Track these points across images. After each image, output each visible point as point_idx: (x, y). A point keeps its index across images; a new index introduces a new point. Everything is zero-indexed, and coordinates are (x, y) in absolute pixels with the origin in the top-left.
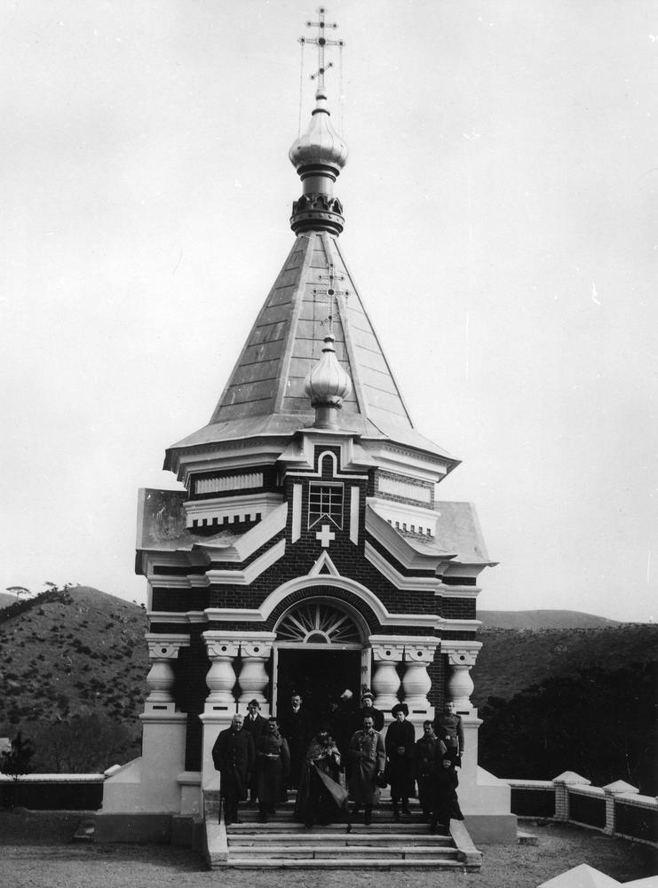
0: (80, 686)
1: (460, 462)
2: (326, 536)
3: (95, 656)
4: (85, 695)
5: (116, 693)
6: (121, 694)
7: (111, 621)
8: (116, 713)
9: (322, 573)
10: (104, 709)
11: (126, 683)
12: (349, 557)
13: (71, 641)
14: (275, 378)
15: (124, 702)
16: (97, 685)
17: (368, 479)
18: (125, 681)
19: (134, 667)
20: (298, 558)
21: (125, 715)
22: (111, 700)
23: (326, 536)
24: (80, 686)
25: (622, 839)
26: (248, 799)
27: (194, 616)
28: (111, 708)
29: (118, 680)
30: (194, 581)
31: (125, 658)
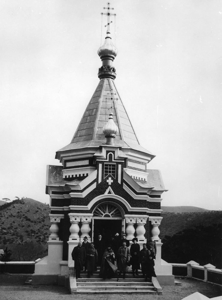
0: (27, 232)
1: (155, 156)
2: (110, 181)
3: (32, 222)
4: (29, 235)
5: (39, 234)
6: (41, 234)
7: (37, 210)
9: (109, 194)
12: (118, 188)
13: (24, 216)
15: (42, 237)
16: (33, 231)
17: (124, 162)
18: (42, 230)
19: (45, 225)
20: (101, 189)
21: (42, 242)
22: (37, 237)
23: (110, 181)
24: (27, 232)
27: (65, 208)
28: (38, 239)
30: (66, 196)
31: (42, 222)
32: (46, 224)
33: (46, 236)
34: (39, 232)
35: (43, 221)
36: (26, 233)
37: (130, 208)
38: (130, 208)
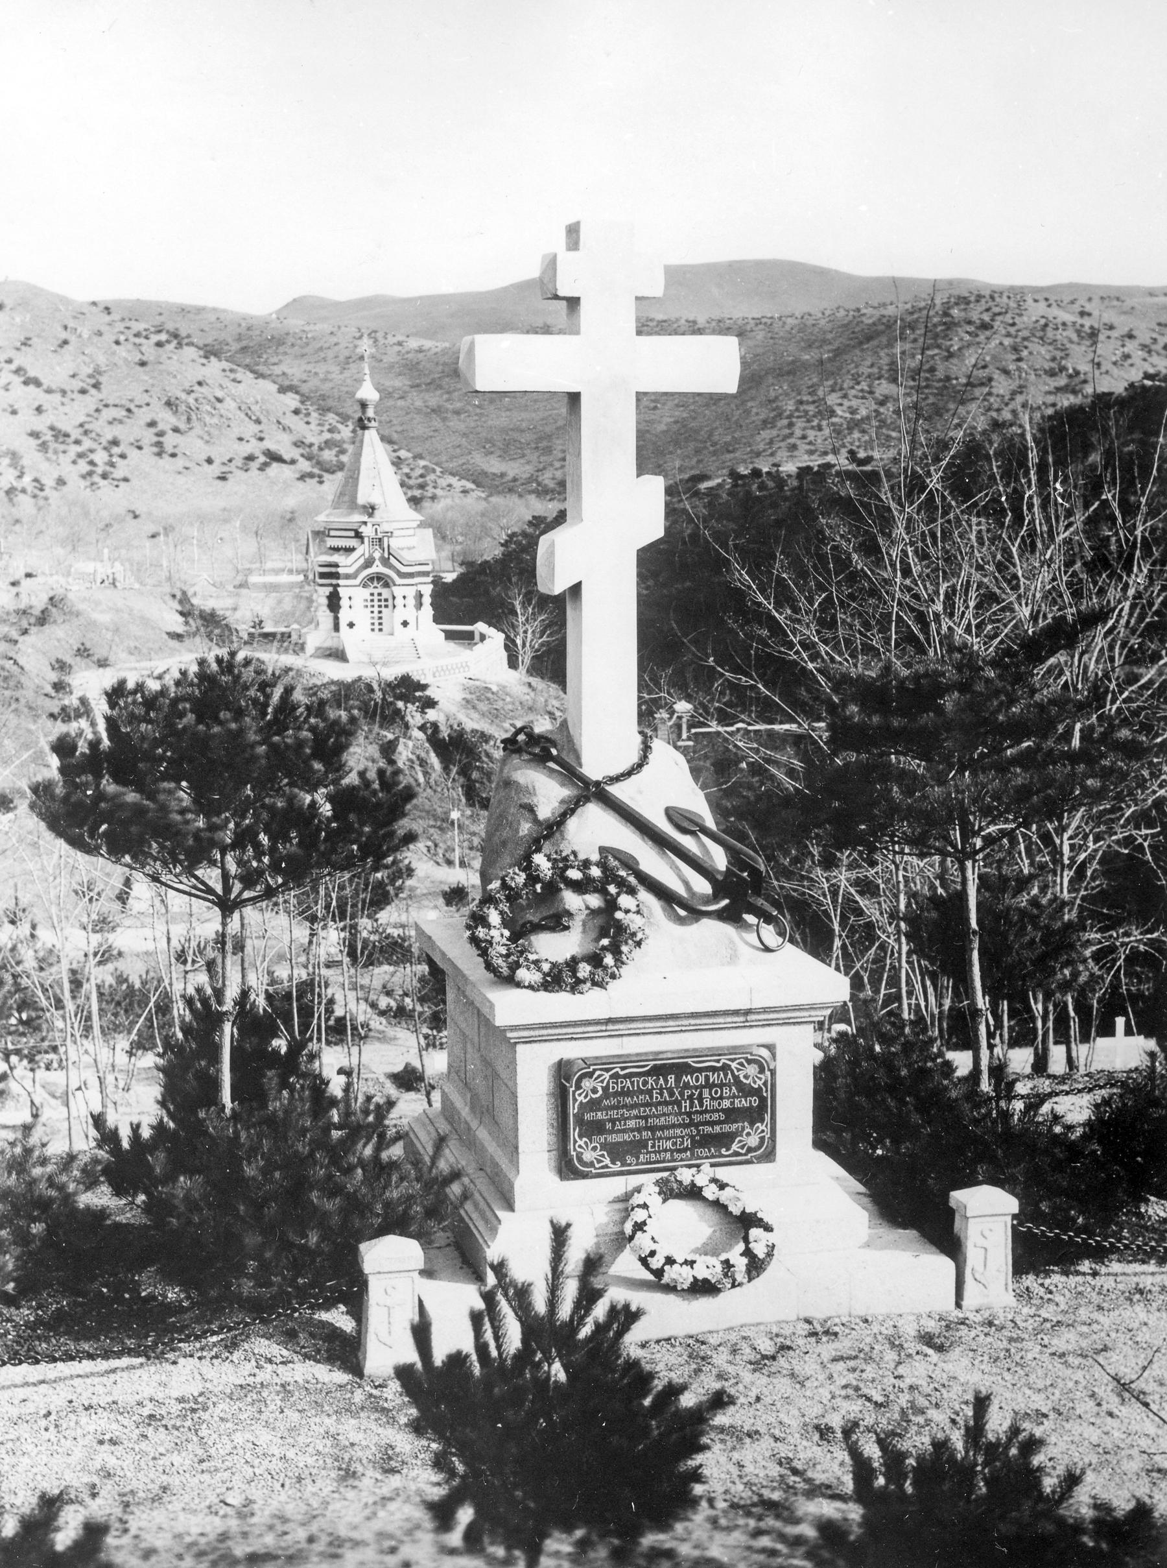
0: (35, 435)
1: (578, 223)
2: (377, 555)
3: (49, 391)
4: (44, 447)
5: (87, 444)
6: (94, 446)
7: (64, 335)
8: (90, 474)
9: (378, 568)
10: (72, 467)
11: (98, 430)
12: (385, 562)
13: (13, 367)
14: (437, 1021)
15: (100, 457)
16: (60, 435)
17: (390, 534)
18: (96, 426)
19: (106, 406)
20: (369, 563)
21: (104, 476)
22: (81, 455)
23: (377, 555)
24: (35, 435)
25: (771, 734)
26: (1078, 726)
27: (334, 582)
28: (83, 467)
29: (87, 426)
30: (333, 570)
31: (93, 391)
32: (110, 402)
33: (116, 450)
34: (86, 433)
35: (96, 386)
36: (33, 443)
37: (398, 580)
38: (398, 580)
